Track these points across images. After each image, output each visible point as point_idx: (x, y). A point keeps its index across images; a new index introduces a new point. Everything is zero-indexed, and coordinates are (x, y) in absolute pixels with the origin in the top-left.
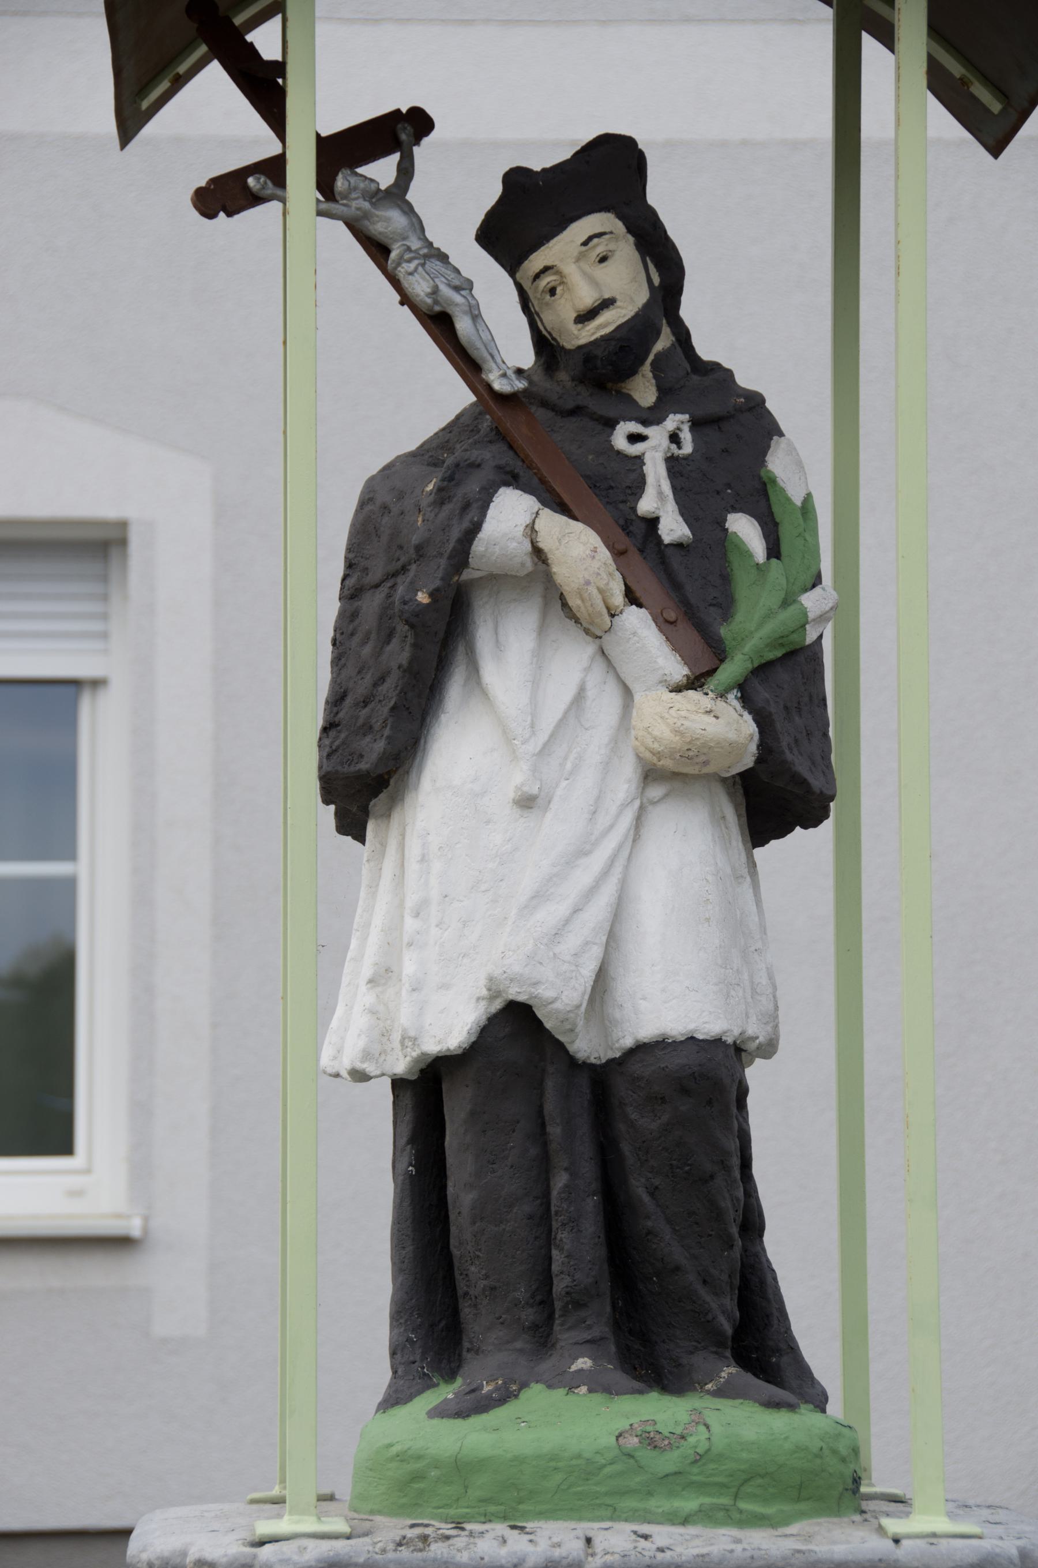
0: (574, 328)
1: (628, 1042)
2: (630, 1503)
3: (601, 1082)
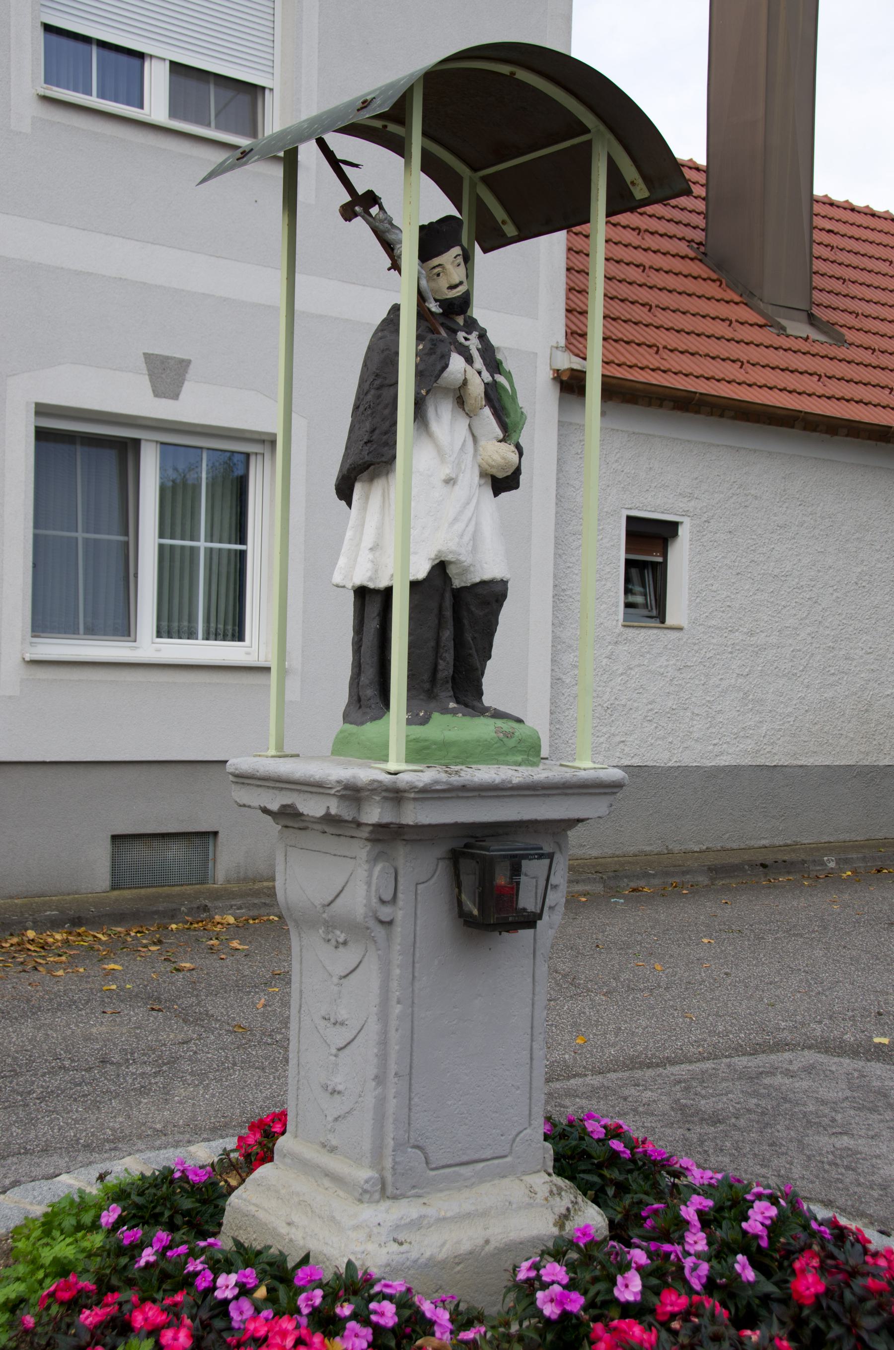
0: (446, 291)
1: (478, 580)
2: (501, 758)
3: (459, 595)
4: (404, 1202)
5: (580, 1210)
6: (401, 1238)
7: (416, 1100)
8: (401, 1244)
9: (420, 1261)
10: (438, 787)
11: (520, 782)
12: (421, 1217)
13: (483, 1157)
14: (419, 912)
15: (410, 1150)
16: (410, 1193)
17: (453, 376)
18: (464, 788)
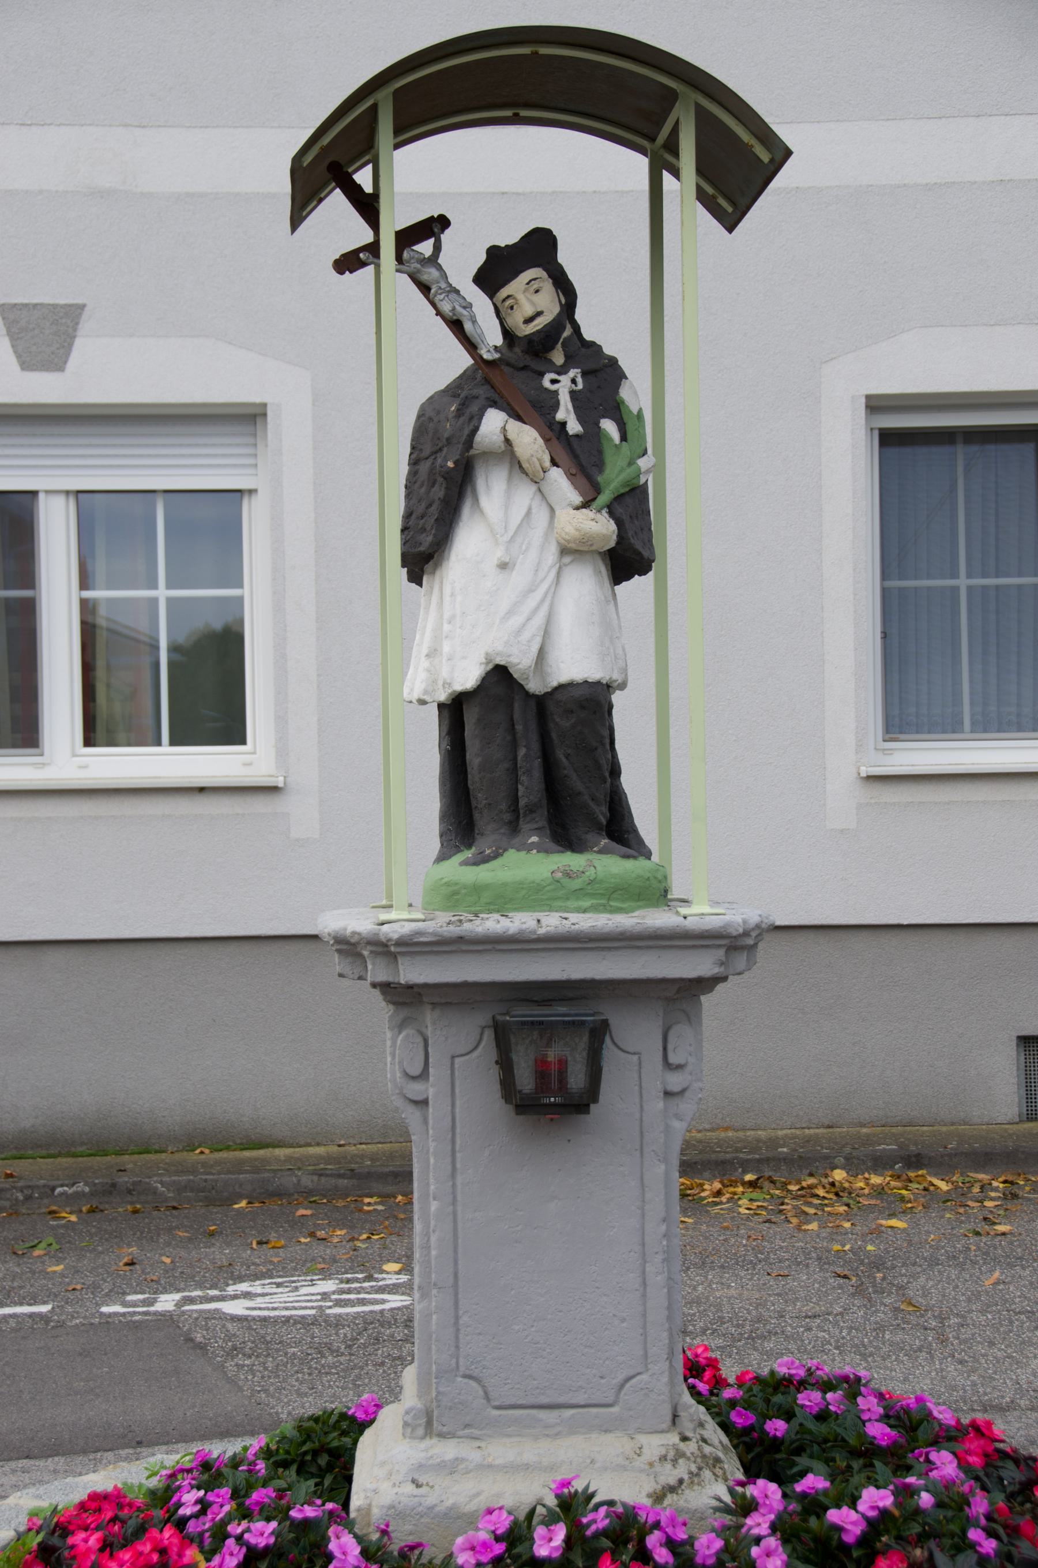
0: (523, 326)
1: (555, 684)
2: (559, 903)
4: (453, 1442)
5: (699, 1484)
6: (421, 1480)
7: (464, 1320)
8: (418, 1486)
9: (438, 1509)
10: (422, 939)
11: (547, 932)
12: (457, 1459)
13: (574, 1401)
14: (457, 1091)
15: (459, 1379)
16: (461, 1433)
17: (487, 440)
18: (461, 939)
